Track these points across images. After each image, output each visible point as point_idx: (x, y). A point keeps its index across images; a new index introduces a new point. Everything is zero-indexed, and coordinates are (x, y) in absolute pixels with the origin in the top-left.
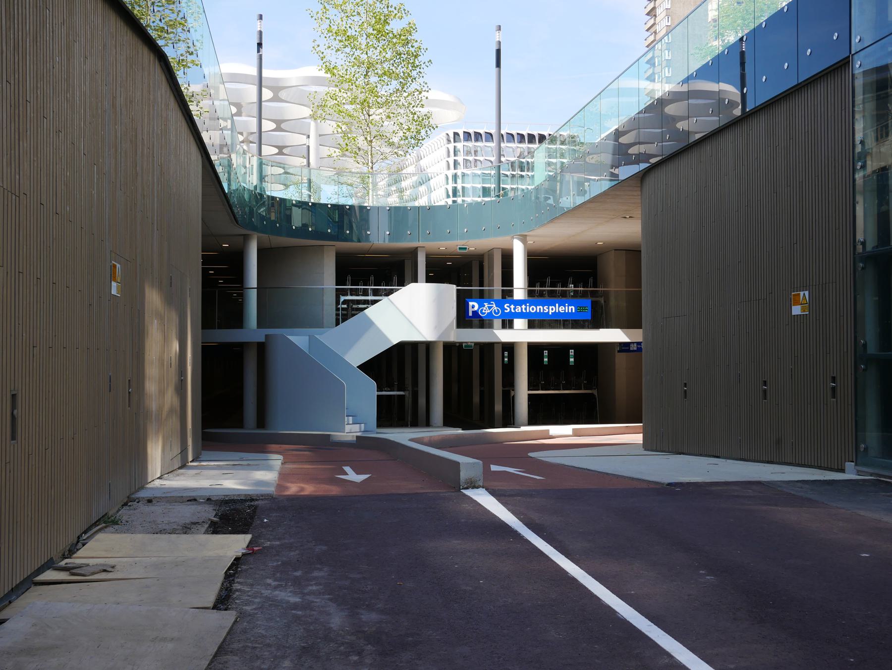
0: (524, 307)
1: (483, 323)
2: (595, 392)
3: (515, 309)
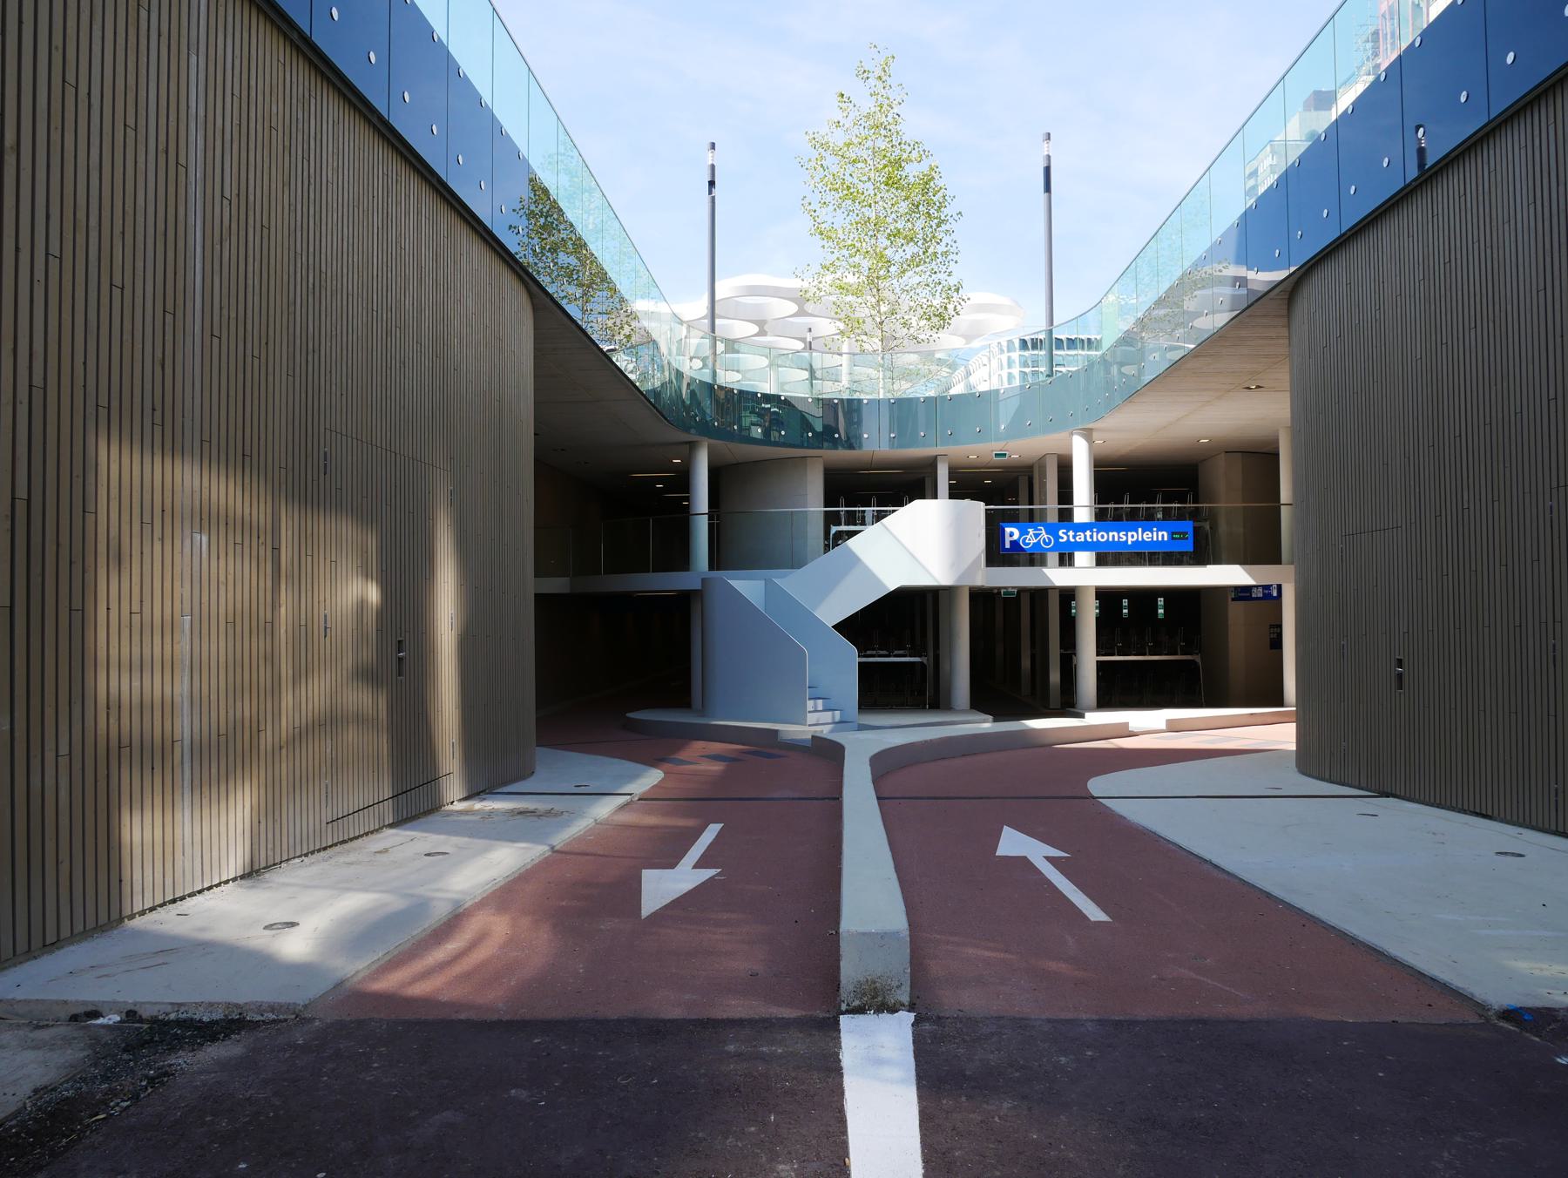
0: (1088, 533)
1: (1034, 559)
2: (1197, 658)
3: (1074, 537)
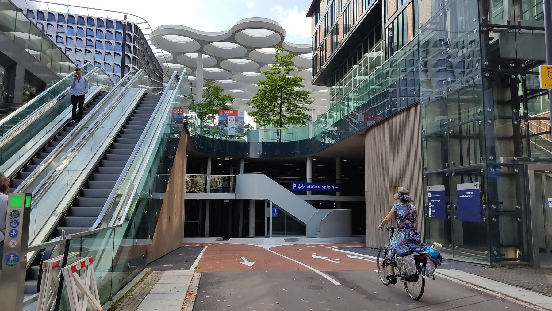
3: (310, 187)
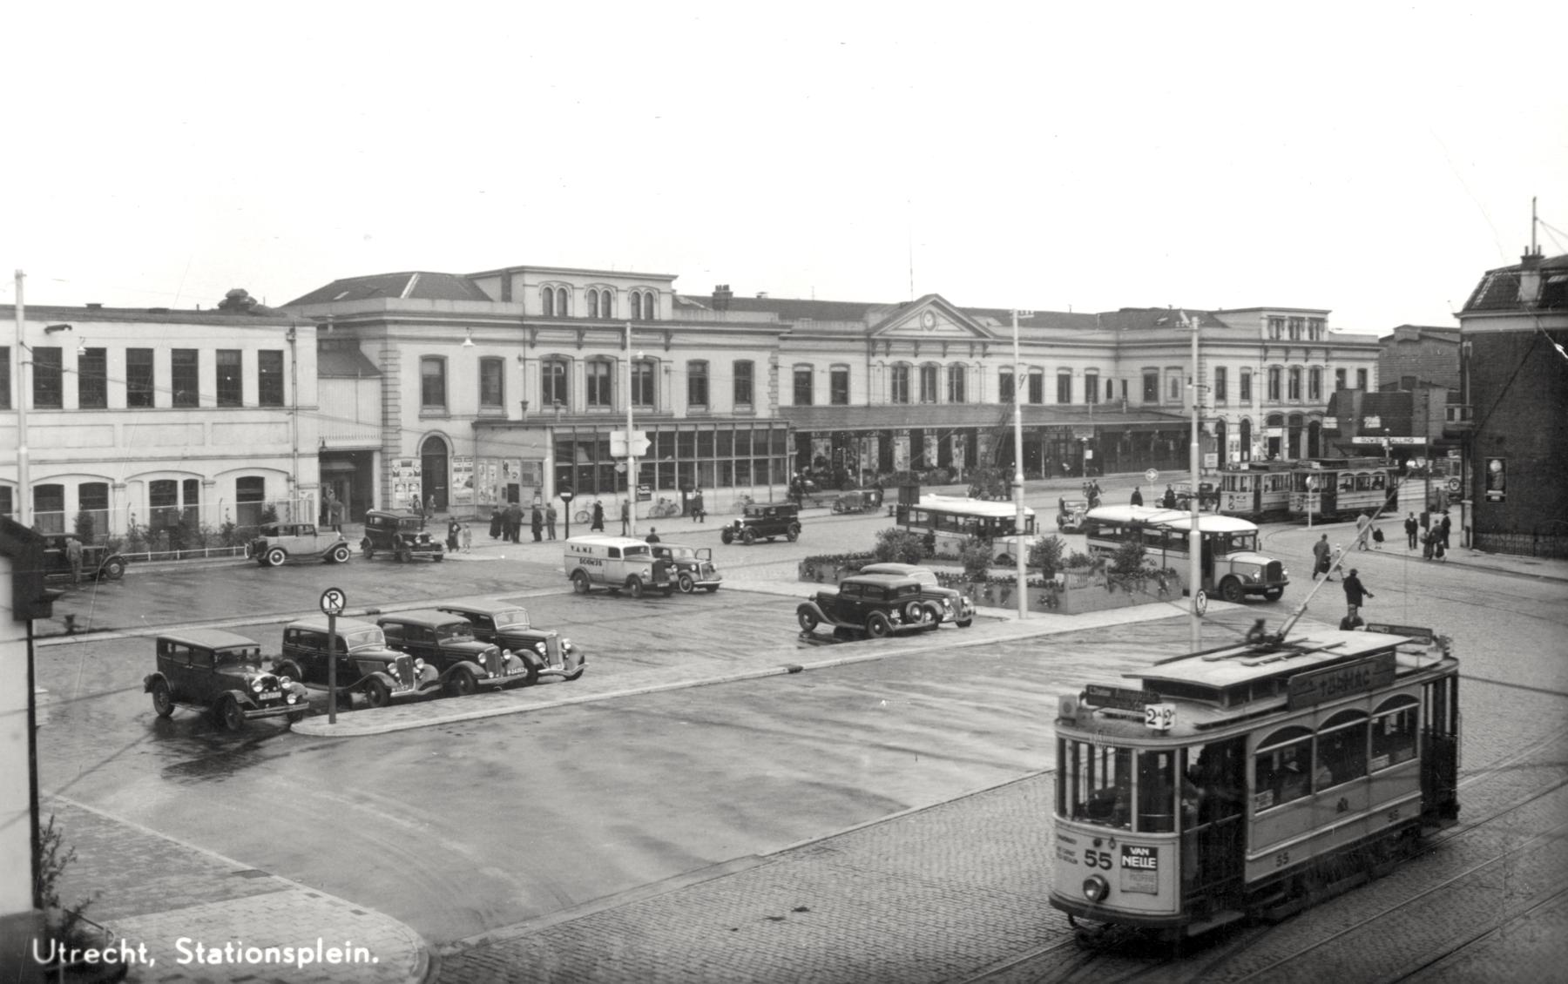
3: (206, 954)
